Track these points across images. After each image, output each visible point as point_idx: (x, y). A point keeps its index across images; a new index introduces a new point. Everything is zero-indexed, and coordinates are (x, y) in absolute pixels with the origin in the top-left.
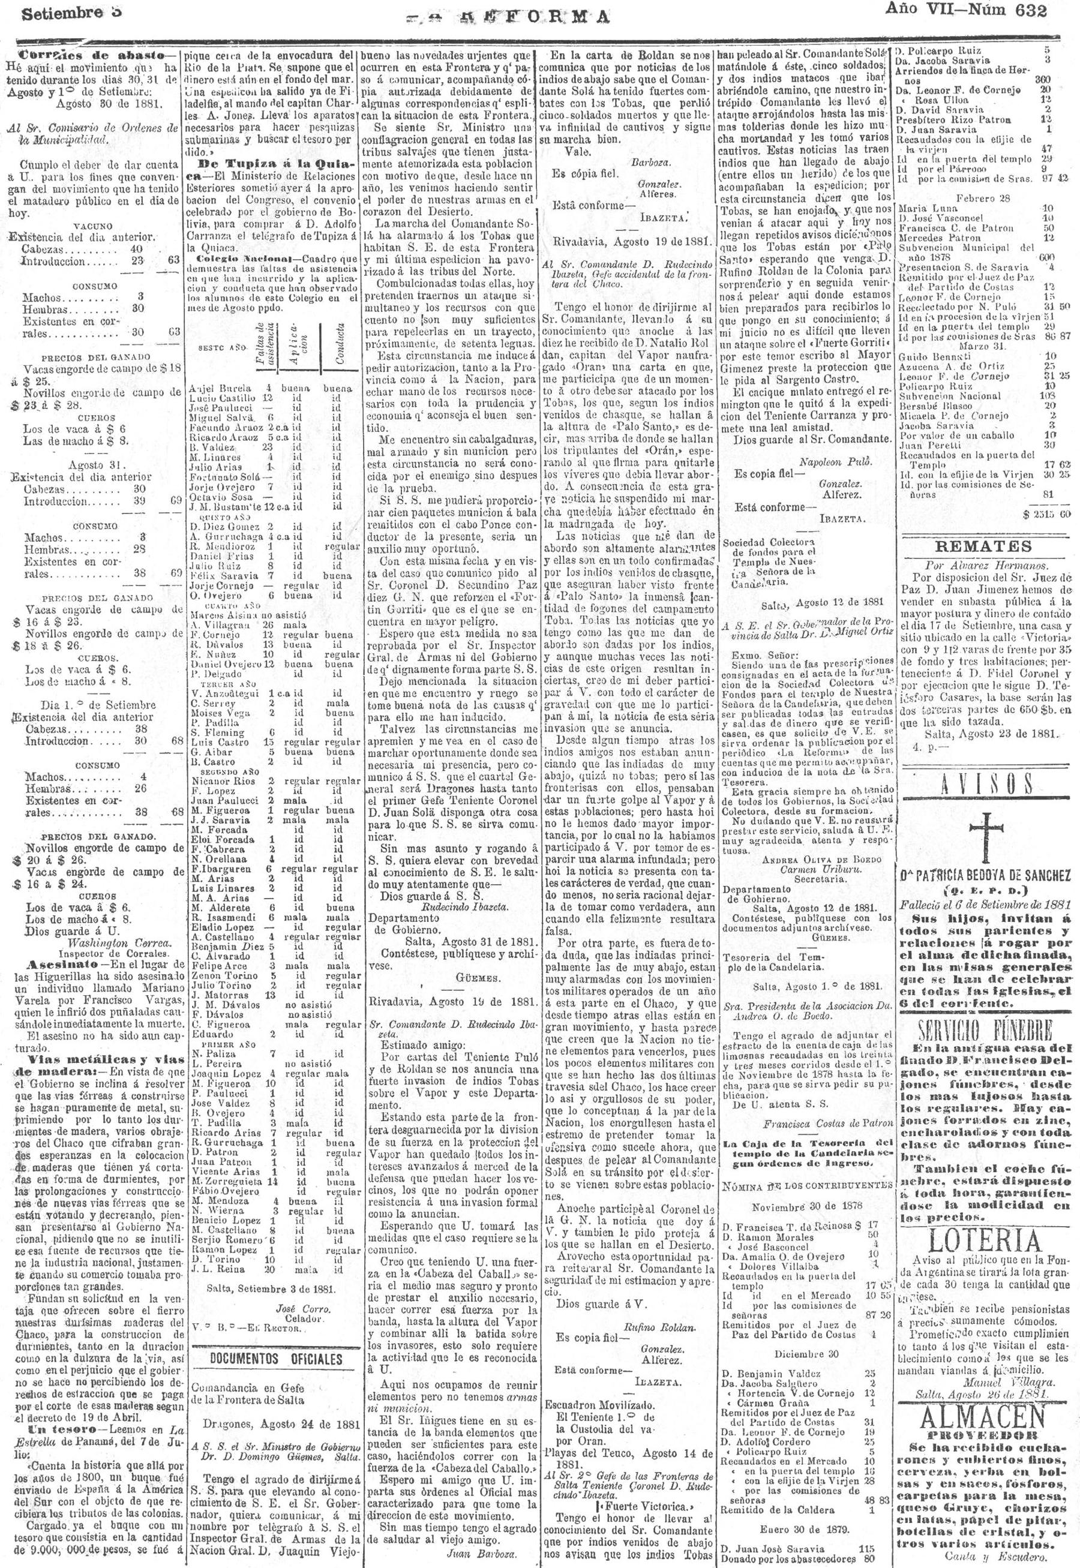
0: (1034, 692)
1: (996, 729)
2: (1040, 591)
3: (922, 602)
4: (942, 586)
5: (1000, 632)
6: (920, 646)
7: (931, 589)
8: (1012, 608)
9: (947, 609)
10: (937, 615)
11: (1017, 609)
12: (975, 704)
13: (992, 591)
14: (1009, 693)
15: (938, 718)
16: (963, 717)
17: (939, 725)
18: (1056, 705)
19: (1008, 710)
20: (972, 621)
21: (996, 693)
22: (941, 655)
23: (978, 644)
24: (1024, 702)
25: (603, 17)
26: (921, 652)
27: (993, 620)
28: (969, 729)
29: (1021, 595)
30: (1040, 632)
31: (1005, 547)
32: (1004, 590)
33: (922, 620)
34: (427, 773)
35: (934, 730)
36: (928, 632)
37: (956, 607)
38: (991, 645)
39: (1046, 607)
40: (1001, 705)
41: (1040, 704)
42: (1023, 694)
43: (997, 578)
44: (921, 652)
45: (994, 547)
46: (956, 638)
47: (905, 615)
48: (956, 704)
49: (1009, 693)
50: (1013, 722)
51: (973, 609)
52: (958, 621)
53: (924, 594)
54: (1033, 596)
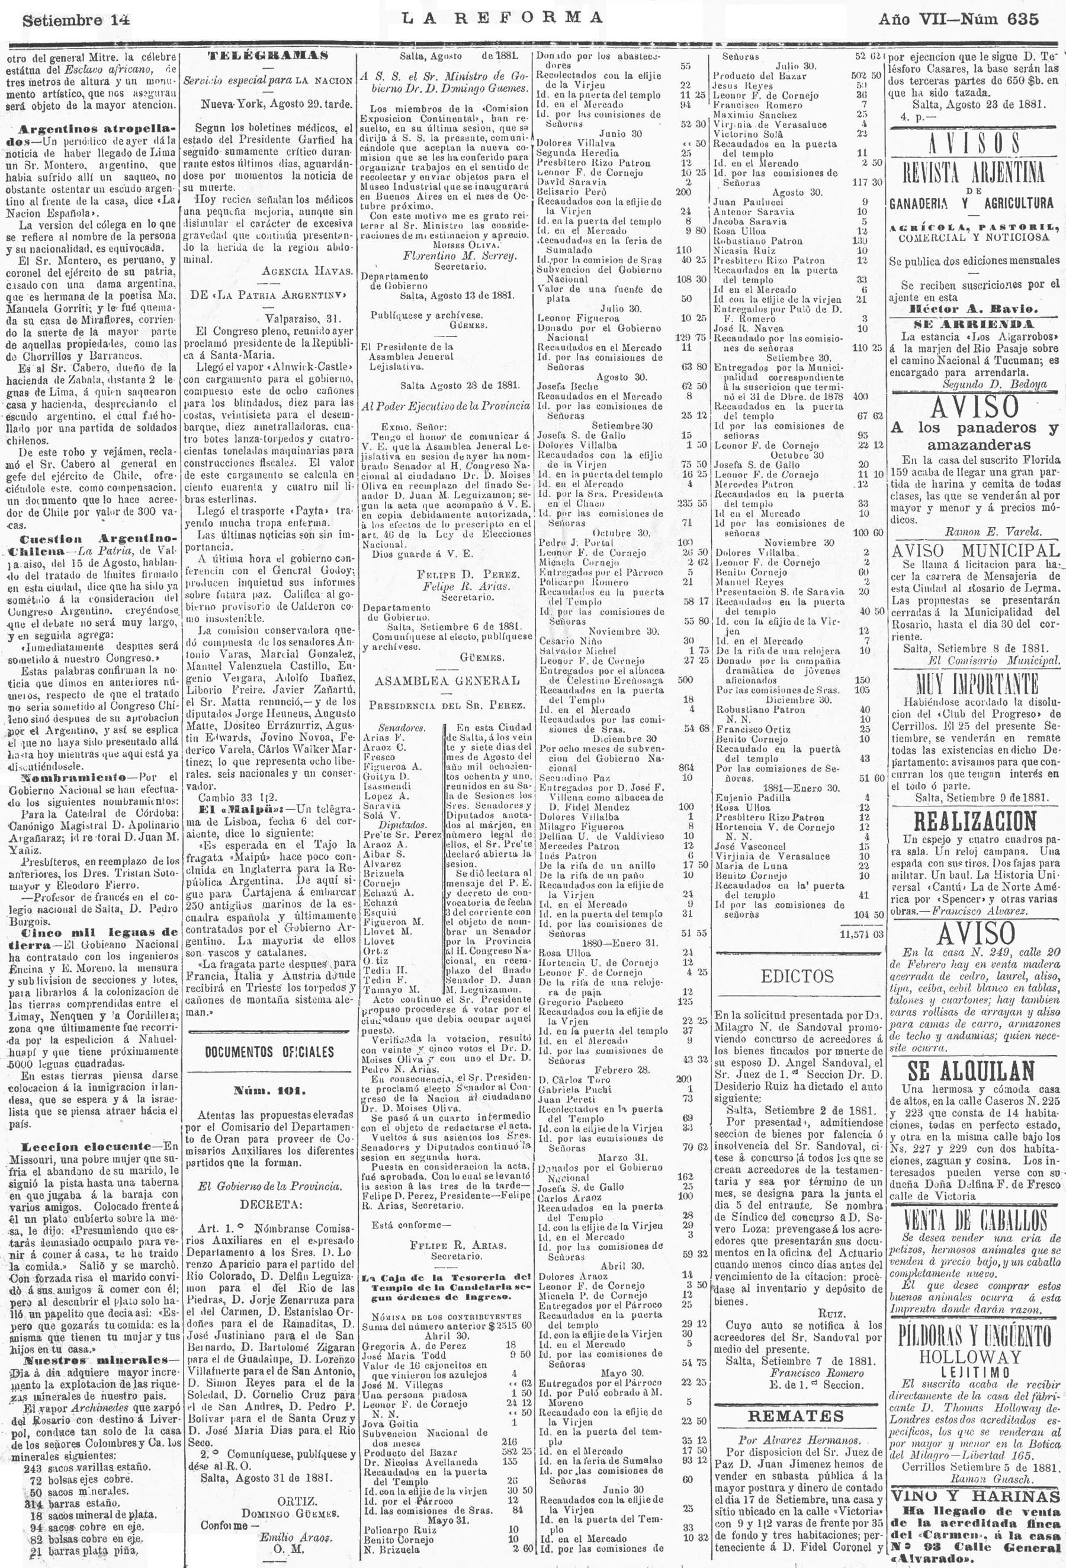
0: (1020, 63)
1: (982, 101)
2: (851, 1465)
3: (735, 1477)
4: (755, 1461)
5: (813, 1506)
6: (734, 1520)
7: (744, 1464)
8: (824, 1482)
9: (761, 1483)
10: (751, 1489)
11: (829, 1483)
12: (961, 76)
13: (805, 1465)
14: (997, 64)
15: (926, 89)
16: (951, 88)
17: (927, 96)
18: (1043, 76)
19: (995, 81)
20: (785, 1495)
21: (983, 64)
22: (755, 1529)
23: (792, 1518)
24: (1011, 73)
25: (597, 18)
26: (735, 1526)
27: (806, 1494)
28: (956, 100)
29: (833, 1470)
30: (852, 1506)
31: (818, 1417)
32: (815, 1465)
33: (736, 1495)
34: (399, 136)
35: (922, 100)
36: (742, 1506)
37: (769, 1481)
38: (804, 1519)
39: (858, 1481)
40: (989, 77)
41: (1027, 75)
42: (1010, 65)
43: (809, 1453)
44: (735, 1526)
45: (806, 1417)
46: (770, 1512)
47: (719, 1489)
48: (944, 76)
49: (997, 64)
50: (999, 93)
51: (787, 1483)
52: (772, 1496)
53: (737, 1469)
54: (846, 1471)
